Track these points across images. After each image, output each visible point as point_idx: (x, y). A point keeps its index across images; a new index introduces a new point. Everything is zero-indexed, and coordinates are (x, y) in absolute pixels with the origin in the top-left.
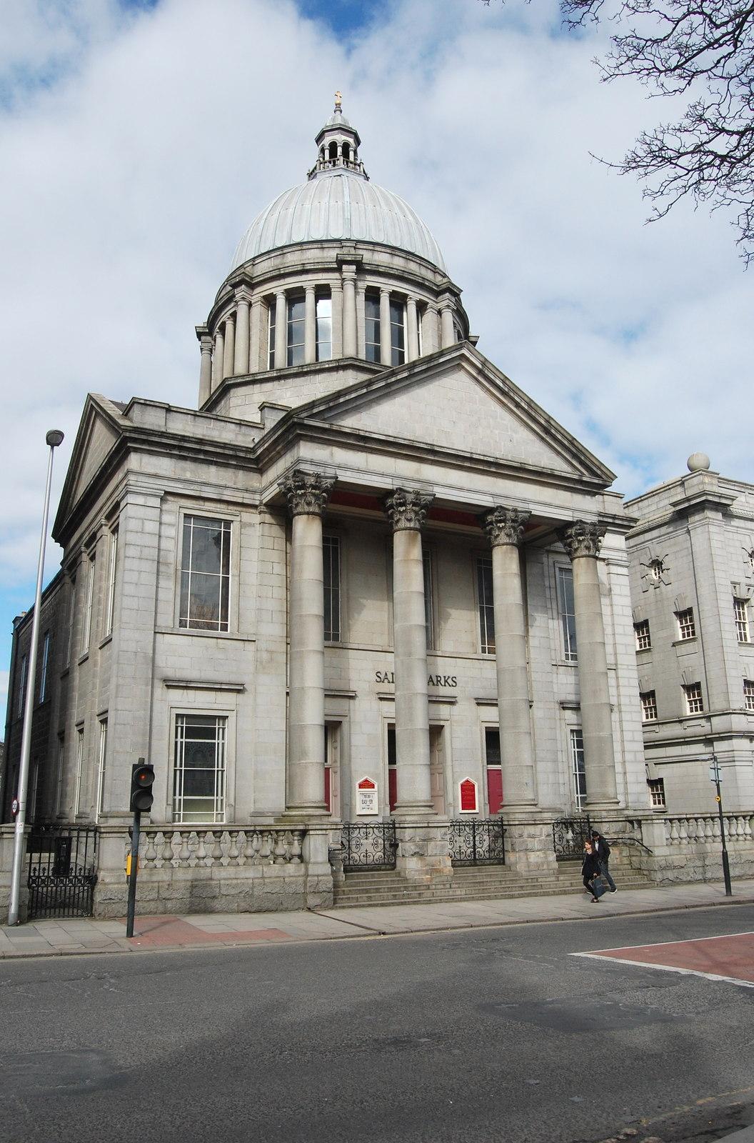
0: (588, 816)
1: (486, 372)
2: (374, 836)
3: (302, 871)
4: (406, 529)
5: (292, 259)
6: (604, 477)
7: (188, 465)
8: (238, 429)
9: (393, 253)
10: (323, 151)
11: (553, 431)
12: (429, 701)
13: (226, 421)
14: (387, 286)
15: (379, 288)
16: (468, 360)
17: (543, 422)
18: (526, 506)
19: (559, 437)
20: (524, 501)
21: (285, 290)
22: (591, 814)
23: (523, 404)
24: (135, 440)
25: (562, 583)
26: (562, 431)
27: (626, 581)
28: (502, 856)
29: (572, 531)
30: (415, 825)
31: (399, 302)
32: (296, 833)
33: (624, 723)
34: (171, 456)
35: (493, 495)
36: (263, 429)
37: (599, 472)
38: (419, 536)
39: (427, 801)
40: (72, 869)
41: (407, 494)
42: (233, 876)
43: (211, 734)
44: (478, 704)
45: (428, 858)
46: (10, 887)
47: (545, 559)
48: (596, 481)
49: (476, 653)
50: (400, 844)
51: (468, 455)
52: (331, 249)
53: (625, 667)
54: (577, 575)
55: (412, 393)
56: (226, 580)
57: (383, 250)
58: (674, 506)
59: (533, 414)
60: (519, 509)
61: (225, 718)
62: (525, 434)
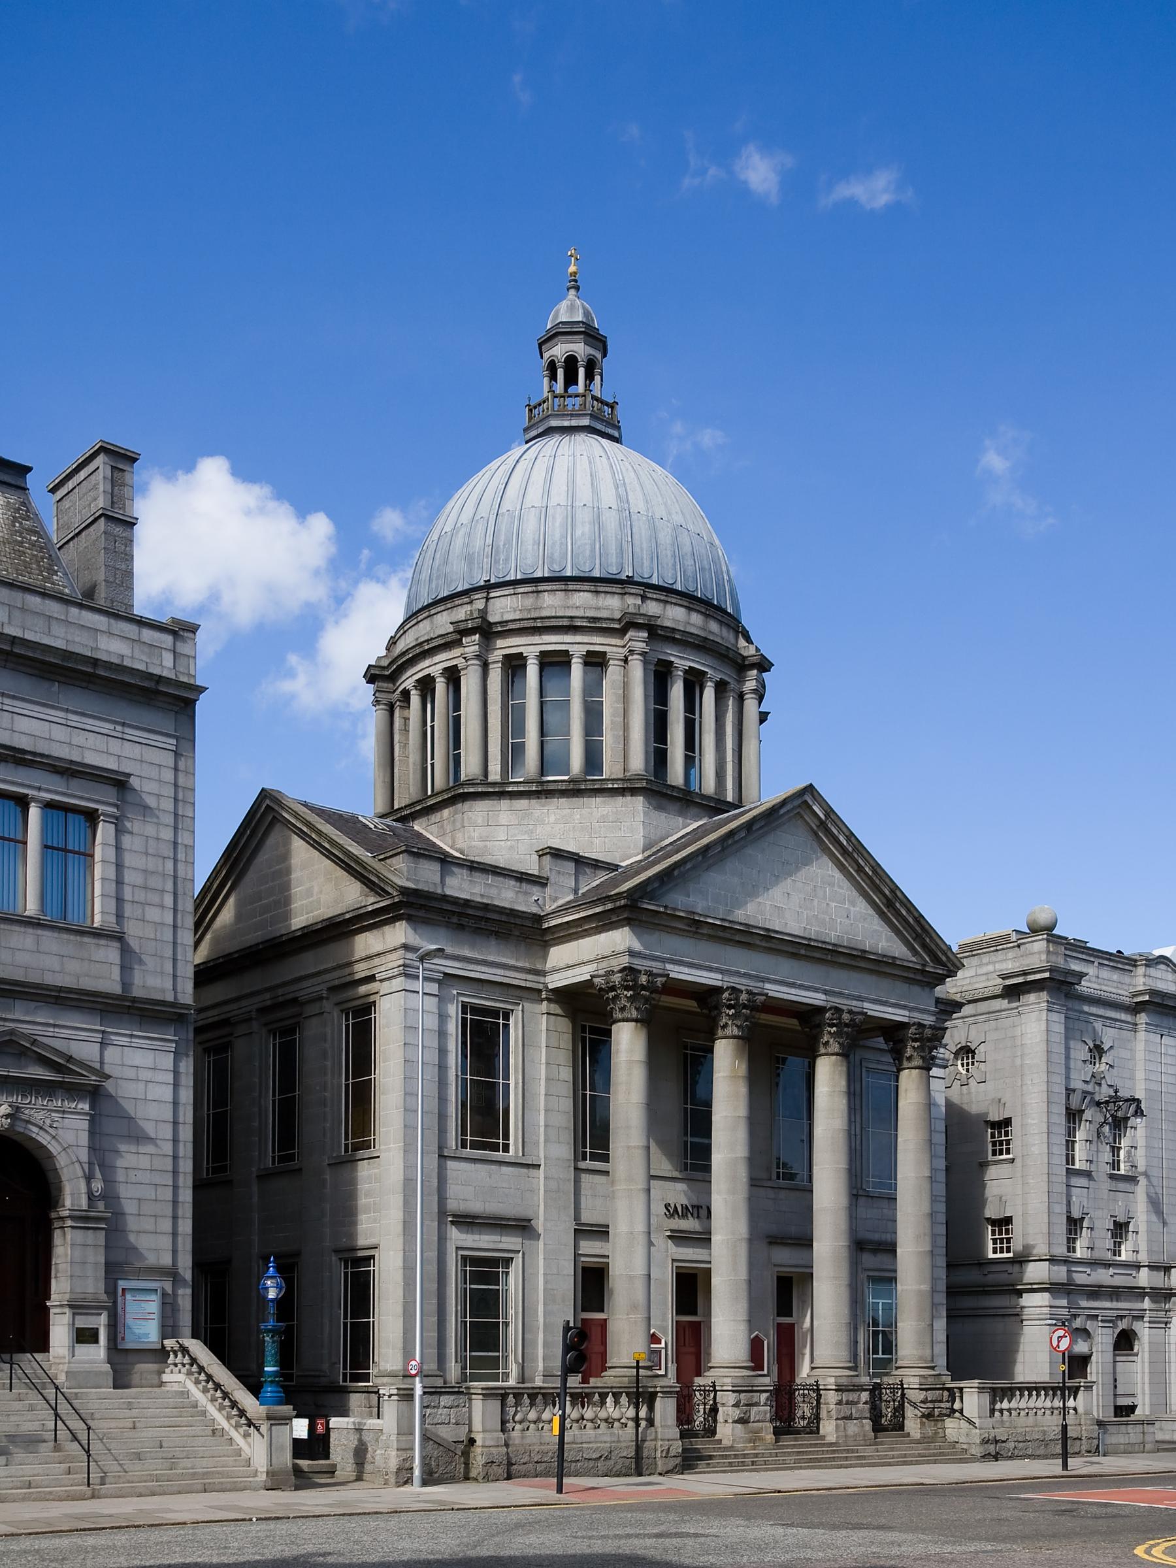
1: (829, 825)
5: (551, 603)
6: (949, 965)
9: (691, 606)
10: (552, 367)
11: (898, 905)
14: (682, 661)
16: (810, 807)
17: (887, 892)
19: (904, 913)
21: (541, 652)
23: (867, 869)
26: (909, 905)
37: (944, 958)
39: (743, 1362)
42: (592, 1439)
43: (493, 1278)
44: (770, 1243)
46: (412, 1449)
50: (720, 1409)
52: (608, 595)
55: (631, 749)
58: (1003, 979)
59: (878, 882)
61: (508, 1262)
62: (862, 907)
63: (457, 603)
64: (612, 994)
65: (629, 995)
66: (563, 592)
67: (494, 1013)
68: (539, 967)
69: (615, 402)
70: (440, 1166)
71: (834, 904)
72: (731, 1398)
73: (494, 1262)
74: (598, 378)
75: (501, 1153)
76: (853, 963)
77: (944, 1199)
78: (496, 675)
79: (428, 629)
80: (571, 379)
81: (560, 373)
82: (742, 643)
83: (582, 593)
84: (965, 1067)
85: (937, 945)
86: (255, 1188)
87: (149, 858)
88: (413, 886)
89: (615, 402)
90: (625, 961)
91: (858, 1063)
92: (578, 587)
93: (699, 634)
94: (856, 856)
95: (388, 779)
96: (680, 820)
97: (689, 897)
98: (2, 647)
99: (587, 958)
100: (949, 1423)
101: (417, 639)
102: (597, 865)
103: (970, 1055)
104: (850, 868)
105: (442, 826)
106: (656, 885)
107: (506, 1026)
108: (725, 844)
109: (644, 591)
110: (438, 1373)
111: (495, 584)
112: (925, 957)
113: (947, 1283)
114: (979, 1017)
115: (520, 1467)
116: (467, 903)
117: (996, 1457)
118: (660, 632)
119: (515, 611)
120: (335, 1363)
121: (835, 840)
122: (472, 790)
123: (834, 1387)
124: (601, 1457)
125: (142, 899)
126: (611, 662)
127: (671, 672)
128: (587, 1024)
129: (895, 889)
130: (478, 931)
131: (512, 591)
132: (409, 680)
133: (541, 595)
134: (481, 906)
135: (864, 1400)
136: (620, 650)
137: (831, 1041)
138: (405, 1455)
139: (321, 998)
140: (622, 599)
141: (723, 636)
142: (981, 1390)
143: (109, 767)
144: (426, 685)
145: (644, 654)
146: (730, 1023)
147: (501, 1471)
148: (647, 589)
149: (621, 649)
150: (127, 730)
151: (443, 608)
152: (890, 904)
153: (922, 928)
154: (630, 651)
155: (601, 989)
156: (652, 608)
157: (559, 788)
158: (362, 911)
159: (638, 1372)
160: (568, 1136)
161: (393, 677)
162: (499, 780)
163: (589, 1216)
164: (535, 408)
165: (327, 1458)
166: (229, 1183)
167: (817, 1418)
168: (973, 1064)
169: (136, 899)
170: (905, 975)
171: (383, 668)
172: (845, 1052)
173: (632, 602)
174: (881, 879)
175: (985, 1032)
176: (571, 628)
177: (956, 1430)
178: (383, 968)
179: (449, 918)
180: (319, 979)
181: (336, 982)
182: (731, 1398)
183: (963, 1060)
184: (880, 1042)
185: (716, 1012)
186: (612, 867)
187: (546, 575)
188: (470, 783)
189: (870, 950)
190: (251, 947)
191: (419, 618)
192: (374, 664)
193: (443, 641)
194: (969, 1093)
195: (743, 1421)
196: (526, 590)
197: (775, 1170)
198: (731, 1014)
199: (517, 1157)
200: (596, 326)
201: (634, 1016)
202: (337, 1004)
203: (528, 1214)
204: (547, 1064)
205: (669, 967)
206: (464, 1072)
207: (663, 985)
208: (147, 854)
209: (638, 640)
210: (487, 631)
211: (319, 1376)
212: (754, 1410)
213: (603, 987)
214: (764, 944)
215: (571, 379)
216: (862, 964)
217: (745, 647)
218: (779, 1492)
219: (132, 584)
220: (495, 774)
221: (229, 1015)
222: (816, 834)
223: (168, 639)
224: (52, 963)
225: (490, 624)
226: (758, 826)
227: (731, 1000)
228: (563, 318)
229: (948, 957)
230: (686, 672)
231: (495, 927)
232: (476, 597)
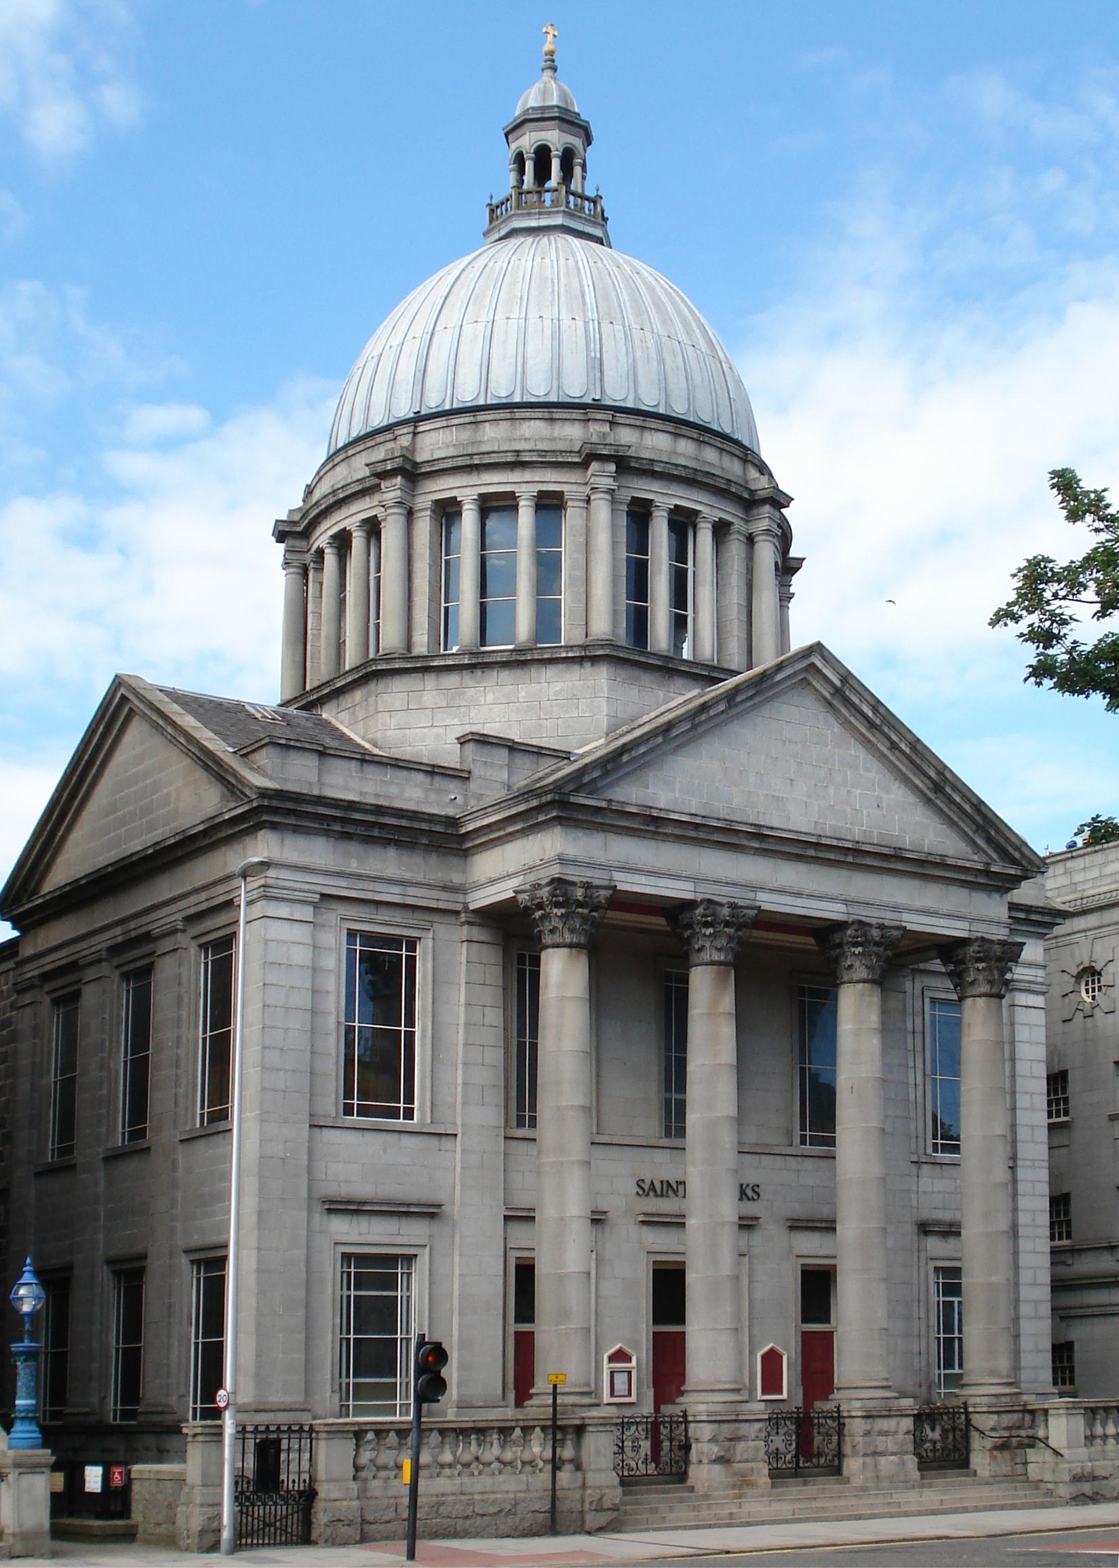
1: (847, 693)
2: (786, 1429)
3: (579, 1482)
4: (713, 963)
6: (1024, 863)
7: (354, 847)
8: (429, 779)
10: (520, 159)
11: (948, 789)
13: (412, 769)
14: (665, 497)
15: (651, 501)
16: (819, 671)
17: (933, 774)
18: (896, 916)
19: (958, 799)
20: (896, 908)
21: (480, 495)
22: (971, 1401)
23: (903, 746)
25: (933, 1022)
27: (1039, 1017)
28: (836, 1462)
30: (719, 1418)
31: (683, 523)
32: (571, 1430)
33: (1021, 1256)
34: (328, 833)
35: (846, 902)
36: (468, 778)
37: (1017, 855)
40: (283, 1481)
41: (719, 908)
42: (488, 1489)
44: (792, 1228)
45: (736, 1465)
47: (908, 984)
48: (1012, 872)
49: (791, 1145)
50: (694, 1446)
52: (567, 423)
53: (1029, 1163)
54: (969, 1025)
59: (919, 761)
60: (887, 923)
61: (410, 1259)
63: (378, 440)
64: (538, 914)
65: (559, 914)
66: (509, 422)
67: (395, 941)
68: (456, 878)
69: (597, 196)
70: (311, 1140)
71: (859, 791)
72: (706, 1431)
73: (391, 1260)
74: (578, 170)
75: (401, 1120)
76: (885, 865)
77: (1047, 1164)
78: (424, 527)
79: (345, 473)
80: (542, 173)
82: (753, 473)
83: (532, 422)
84: (1091, 994)
85: (1007, 839)
86: (101, 1174)
88: (278, 787)
89: (597, 196)
90: (555, 871)
91: (918, 992)
92: (528, 415)
93: (689, 465)
94: (886, 729)
95: (299, 658)
96: (661, 694)
99: (512, 870)
100: (1032, 1455)
102: (539, 752)
103: (1096, 978)
104: (879, 745)
105: (354, 713)
106: (596, 774)
107: (411, 961)
108: (697, 720)
109: (613, 416)
110: (502, 1403)
111: (426, 415)
112: (76, 804)
113: (1052, 1275)
114: (289, 892)
115: (381, 1527)
116: (352, 806)
117: (1094, 1498)
118: (633, 465)
119: (448, 447)
120: (183, 1396)
121: (855, 709)
122: (384, 667)
123: (859, 1414)
124: (500, 1511)
126: (570, 504)
127: (651, 513)
128: (527, 954)
129: (942, 770)
130: (368, 840)
131: (444, 424)
132: (322, 537)
133: (481, 426)
134: (372, 808)
135: (905, 1429)
136: (581, 489)
137: (857, 964)
138: (211, 1511)
139: (175, 931)
141: (724, 466)
142: (1070, 1410)
144: (342, 541)
145: (611, 491)
146: (708, 945)
147: (354, 1532)
148: (618, 413)
149: (583, 487)
151: (362, 447)
152: (938, 788)
153: (984, 817)
154: (592, 489)
155: (526, 908)
156: (626, 436)
157: (499, 659)
158: (218, 820)
159: (555, 1400)
160: (496, 1097)
161: (306, 534)
162: (426, 654)
163: (522, 1200)
164: (497, 207)
165: (129, 1517)
166: (72, 1168)
167: (840, 1455)
168: (1100, 989)
170: (963, 877)
171: (295, 523)
172: (876, 977)
173: (597, 430)
175: (1114, 948)
176: (518, 464)
177: (1040, 1465)
180: (173, 908)
181: (193, 911)
182: (706, 1431)
183: (1087, 984)
184: (937, 965)
185: (689, 932)
186: (566, 756)
187: (489, 402)
188: (387, 658)
189: (911, 848)
190: (99, 870)
191: (335, 462)
192: (285, 518)
193: (360, 487)
194: (1095, 1026)
195: (722, 1460)
196: (462, 421)
197: (930, 1141)
198: (708, 933)
199: (422, 1123)
200: (576, 111)
201: (568, 941)
202: (194, 938)
203: (441, 1197)
204: (468, 1004)
205: (618, 876)
206: (349, 1016)
207: (607, 899)
209: (602, 475)
211: (162, 1413)
212: (741, 1445)
213: (529, 904)
214: (756, 845)
215: (542, 173)
216: (900, 866)
217: (754, 479)
218: (728, 1552)
220: (421, 644)
221: (77, 956)
222: (830, 704)
225: (416, 465)
226: (745, 697)
227: (707, 916)
228: (533, 103)
230: (671, 512)
231: (394, 834)
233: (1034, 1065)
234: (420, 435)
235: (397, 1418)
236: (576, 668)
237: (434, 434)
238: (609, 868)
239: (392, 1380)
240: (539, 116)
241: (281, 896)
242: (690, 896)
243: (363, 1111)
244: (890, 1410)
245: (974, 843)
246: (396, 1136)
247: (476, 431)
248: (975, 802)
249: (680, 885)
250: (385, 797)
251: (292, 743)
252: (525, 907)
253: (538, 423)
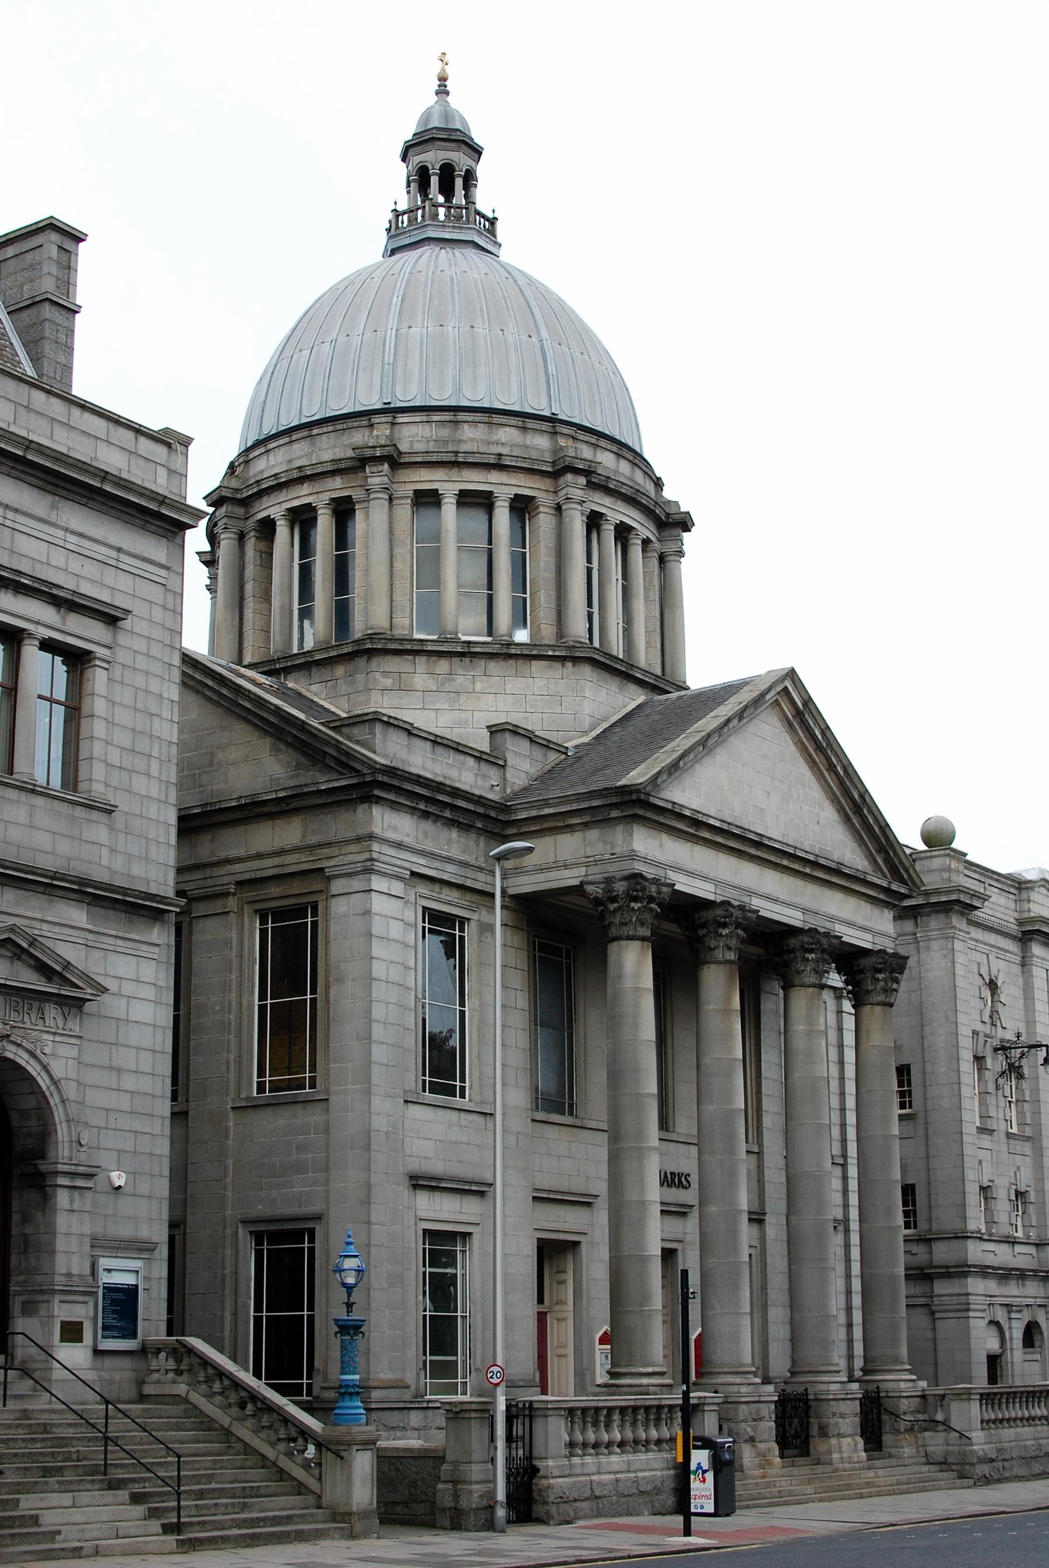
0: (878, 1388)
6: (910, 883)
9: (620, 452)
11: (865, 811)
12: (534, 1197)
14: (617, 512)
17: (856, 797)
18: (828, 925)
20: (832, 918)
21: (461, 491)
24: (383, 786)
29: (793, 942)
34: (413, 810)
35: (805, 911)
37: (905, 876)
38: (650, 944)
51: (812, 858)
56: (462, 1014)
57: (609, 447)
62: (829, 814)
63: (350, 425)
80: (447, 190)
81: (434, 181)
83: (507, 429)
87: (138, 715)
95: (236, 623)
97: (685, 792)
98: (3, 446)
101: (290, 461)
125: (129, 766)
131: (425, 419)
133: (460, 426)
139: (226, 894)
140: (551, 438)
143: (103, 599)
150: (123, 558)
151: (330, 429)
169: (124, 765)
174: (851, 781)
176: (499, 466)
178: (332, 862)
179: (417, 804)
181: (247, 876)
185: (705, 931)
196: (442, 418)
208: (136, 709)
210: (395, 461)
219: (71, 381)
222: (790, 724)
223: (161, 451)
224: (42, 840)
229: (909, 874)
232: (378, 421)
233: (143, 1055)
234: (397, 426)
235: (460, 1398)
236: (558, 665)
237: (412, 427)
238: (665, 866)
239: (453, 1358)
240: (446, 137)
241: (383, 870)
242: (711, 897)
243: (275, 1087)
244: (847, 1394)
245: (875, 862)
246: (456, 1113)
247: (456, 429)
248: (883, 824)
249: (698, 883)
250: (450, 779)
251: (392, 721)
252: (594, 898)
253: (513, 430)
